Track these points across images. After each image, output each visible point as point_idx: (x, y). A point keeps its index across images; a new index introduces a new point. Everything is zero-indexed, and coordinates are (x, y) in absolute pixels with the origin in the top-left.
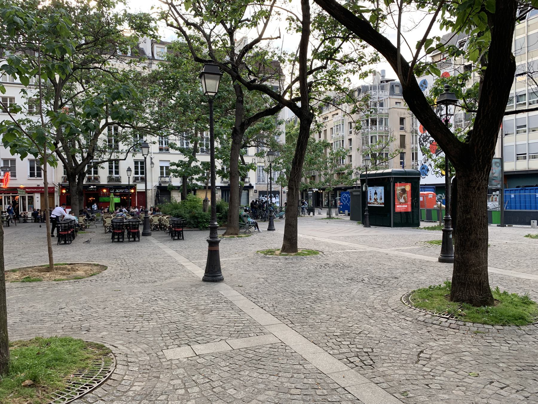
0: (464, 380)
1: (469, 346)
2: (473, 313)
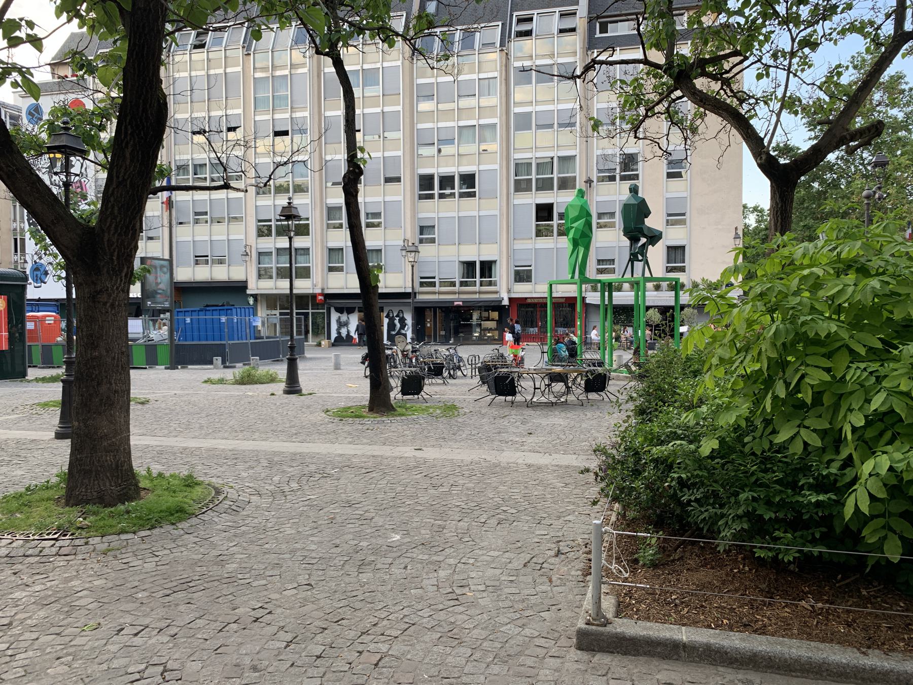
0: (72, 643)
1: (90, 579)
2: (103, 519)
